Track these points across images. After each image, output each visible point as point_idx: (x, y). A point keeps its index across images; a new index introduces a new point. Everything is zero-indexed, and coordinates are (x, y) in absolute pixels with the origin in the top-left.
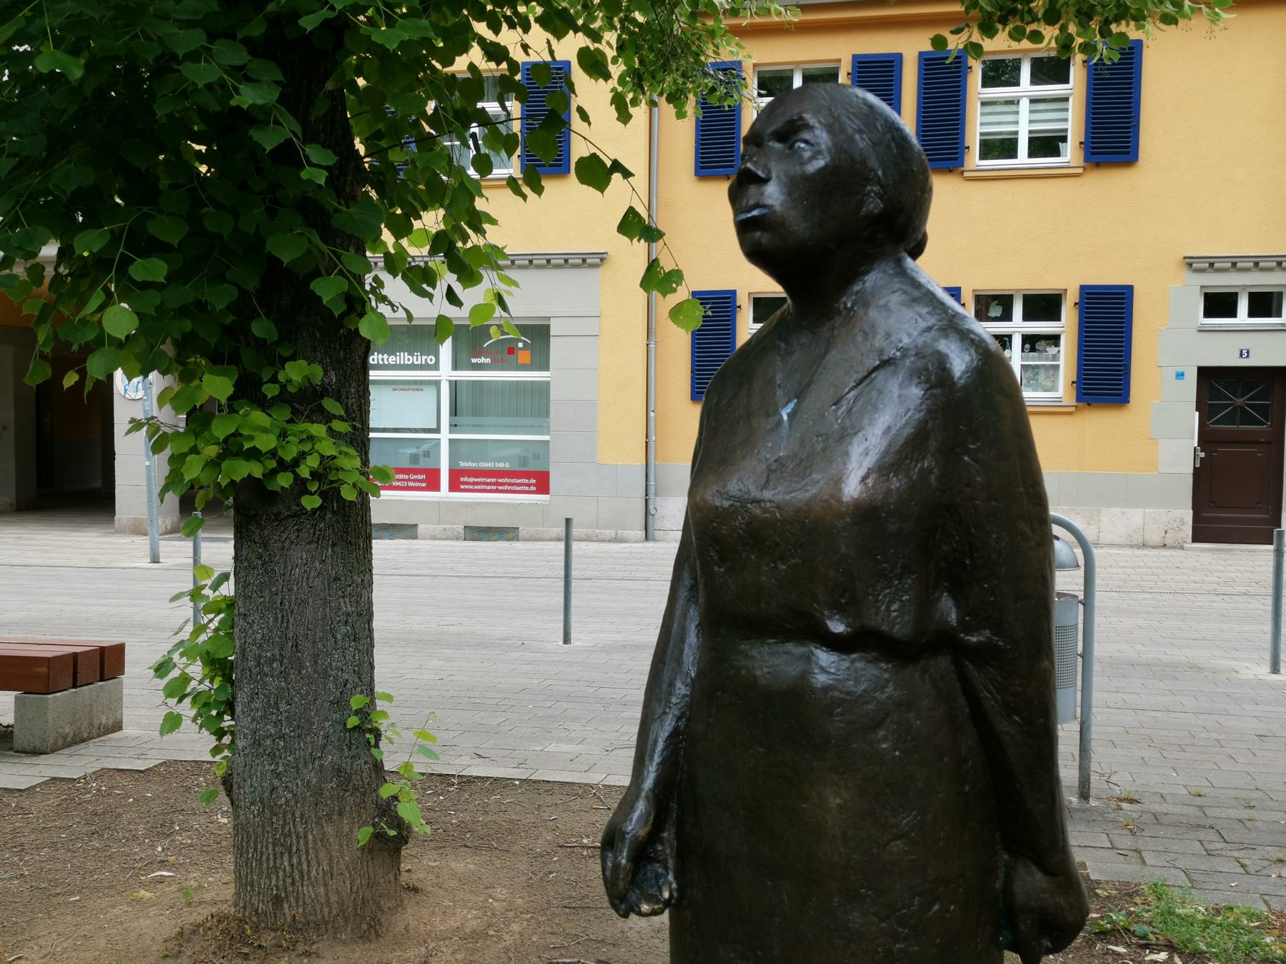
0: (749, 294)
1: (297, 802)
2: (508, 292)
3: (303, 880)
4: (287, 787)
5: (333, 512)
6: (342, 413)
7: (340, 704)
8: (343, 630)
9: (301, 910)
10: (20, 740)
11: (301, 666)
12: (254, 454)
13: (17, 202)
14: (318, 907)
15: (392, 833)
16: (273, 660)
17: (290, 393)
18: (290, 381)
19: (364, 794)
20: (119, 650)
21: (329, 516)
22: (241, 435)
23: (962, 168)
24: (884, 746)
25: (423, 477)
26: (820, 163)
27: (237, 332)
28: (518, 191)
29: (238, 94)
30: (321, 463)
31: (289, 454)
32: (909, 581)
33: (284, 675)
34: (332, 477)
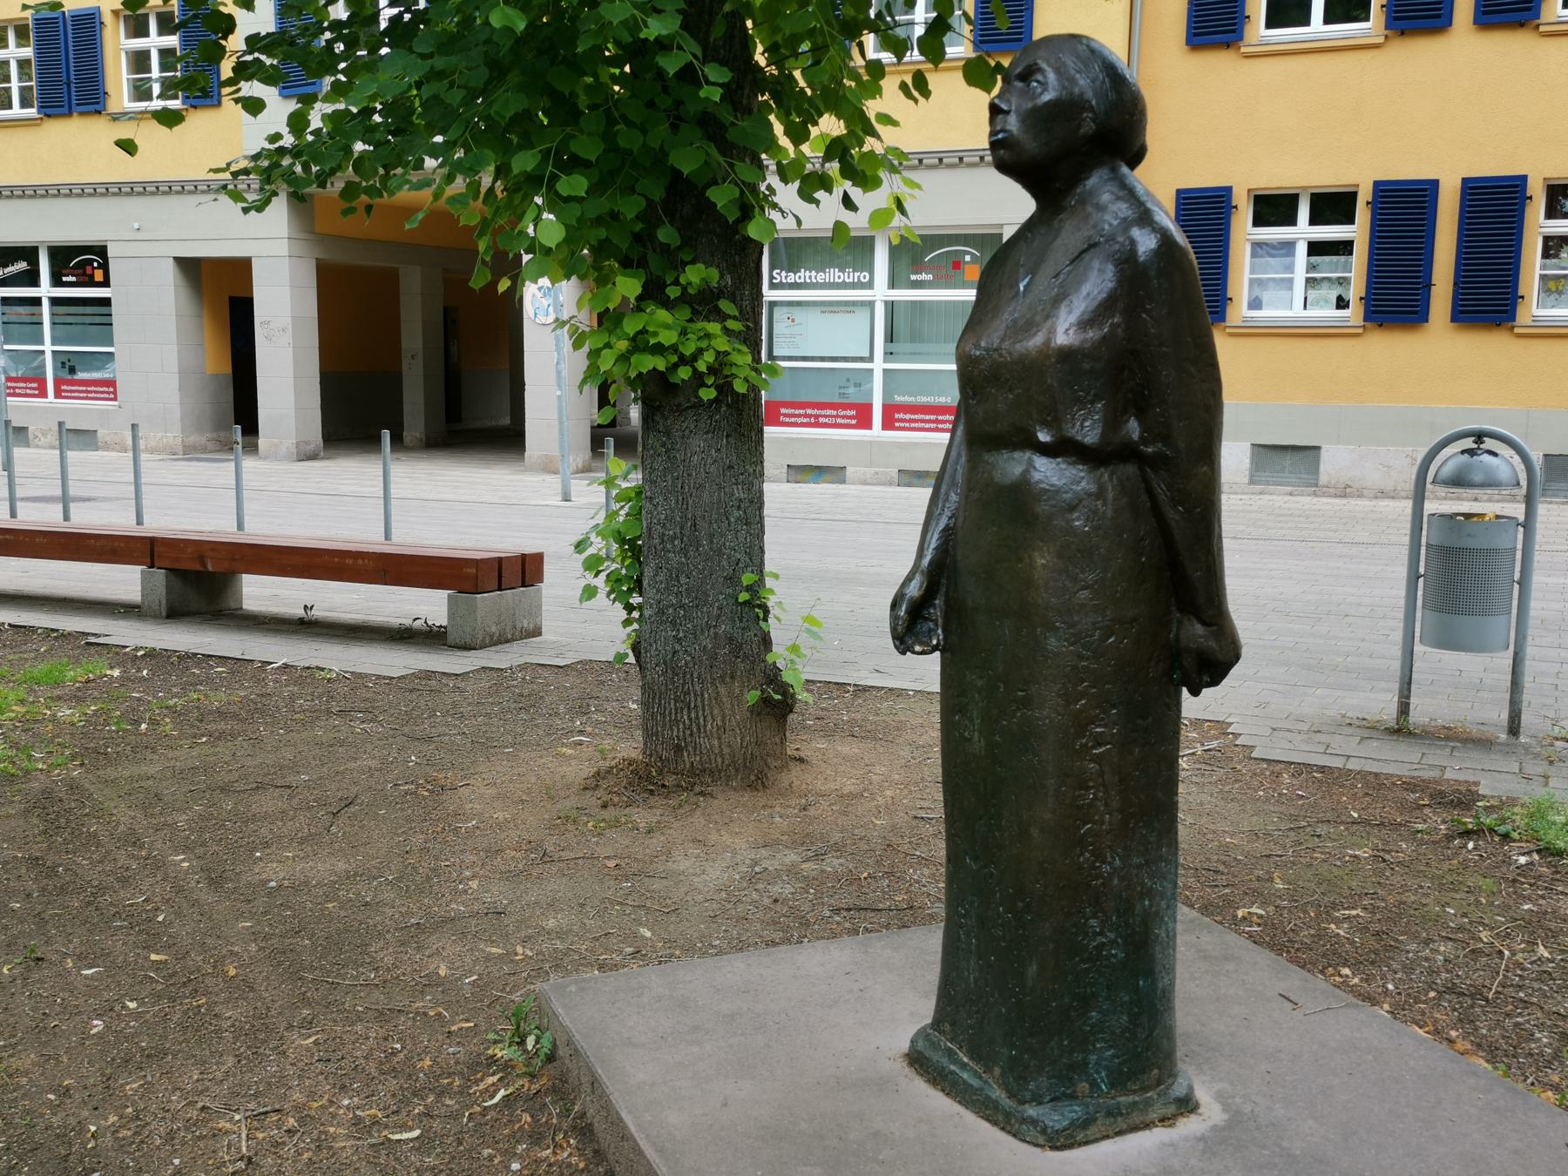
0: (1249, 190)
1: (694, 664)
2: (911, 195)
3: (700, 732)
4: (686, 651)
5: (728, 405)
6: (737, 313)
7: (733, 580)
8: (736, 514)
9: (698, 759)
10: (451, 639)
11: (699, 545)
12: (659, 349)
13: (467, 127)
14: (713, 757)
15: (778, 697)
16: (674, 538)
17: (690, 294)
18: (689, 284)
19: (753, 662)
20: (538, 559)
21: (724, 409)
22: (647, 331)
23: (1538, 21)
24: (1077, 523)
25: (853, 413)
26: (1047, 97)
27: (643, 239)
28: (909, 95)
29: (647, 27)
30: (716, 359)
31: (688, 349)
32: (1100, 405)
33: (684, 551)
34: (726, 372)
